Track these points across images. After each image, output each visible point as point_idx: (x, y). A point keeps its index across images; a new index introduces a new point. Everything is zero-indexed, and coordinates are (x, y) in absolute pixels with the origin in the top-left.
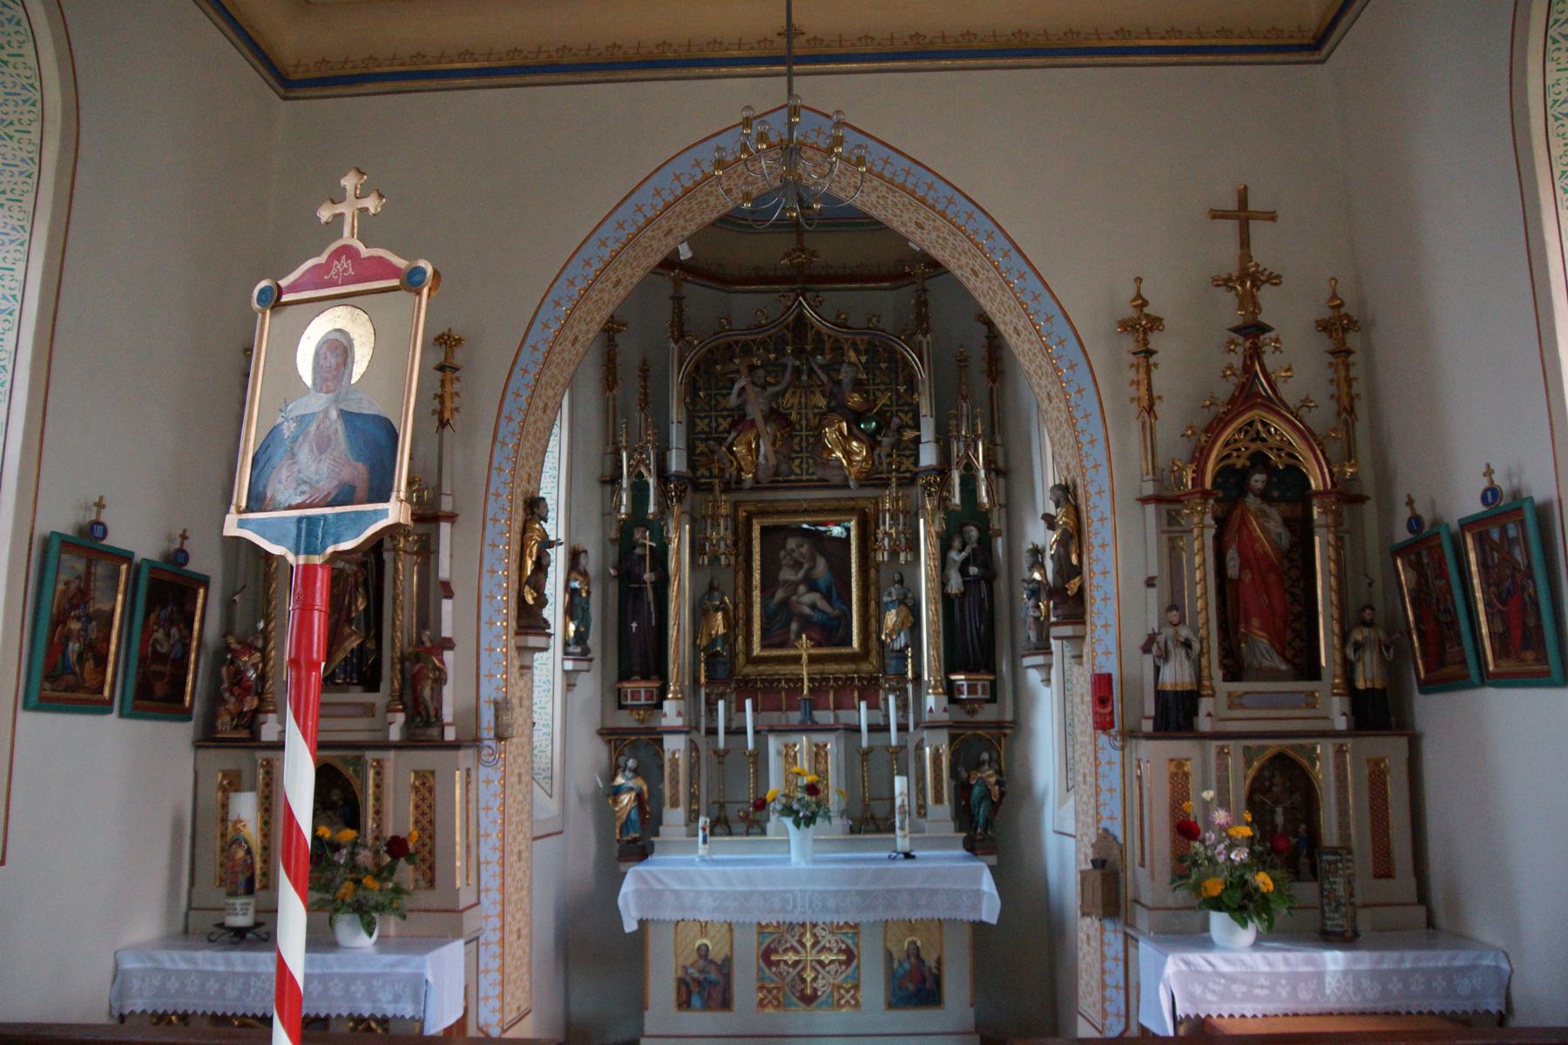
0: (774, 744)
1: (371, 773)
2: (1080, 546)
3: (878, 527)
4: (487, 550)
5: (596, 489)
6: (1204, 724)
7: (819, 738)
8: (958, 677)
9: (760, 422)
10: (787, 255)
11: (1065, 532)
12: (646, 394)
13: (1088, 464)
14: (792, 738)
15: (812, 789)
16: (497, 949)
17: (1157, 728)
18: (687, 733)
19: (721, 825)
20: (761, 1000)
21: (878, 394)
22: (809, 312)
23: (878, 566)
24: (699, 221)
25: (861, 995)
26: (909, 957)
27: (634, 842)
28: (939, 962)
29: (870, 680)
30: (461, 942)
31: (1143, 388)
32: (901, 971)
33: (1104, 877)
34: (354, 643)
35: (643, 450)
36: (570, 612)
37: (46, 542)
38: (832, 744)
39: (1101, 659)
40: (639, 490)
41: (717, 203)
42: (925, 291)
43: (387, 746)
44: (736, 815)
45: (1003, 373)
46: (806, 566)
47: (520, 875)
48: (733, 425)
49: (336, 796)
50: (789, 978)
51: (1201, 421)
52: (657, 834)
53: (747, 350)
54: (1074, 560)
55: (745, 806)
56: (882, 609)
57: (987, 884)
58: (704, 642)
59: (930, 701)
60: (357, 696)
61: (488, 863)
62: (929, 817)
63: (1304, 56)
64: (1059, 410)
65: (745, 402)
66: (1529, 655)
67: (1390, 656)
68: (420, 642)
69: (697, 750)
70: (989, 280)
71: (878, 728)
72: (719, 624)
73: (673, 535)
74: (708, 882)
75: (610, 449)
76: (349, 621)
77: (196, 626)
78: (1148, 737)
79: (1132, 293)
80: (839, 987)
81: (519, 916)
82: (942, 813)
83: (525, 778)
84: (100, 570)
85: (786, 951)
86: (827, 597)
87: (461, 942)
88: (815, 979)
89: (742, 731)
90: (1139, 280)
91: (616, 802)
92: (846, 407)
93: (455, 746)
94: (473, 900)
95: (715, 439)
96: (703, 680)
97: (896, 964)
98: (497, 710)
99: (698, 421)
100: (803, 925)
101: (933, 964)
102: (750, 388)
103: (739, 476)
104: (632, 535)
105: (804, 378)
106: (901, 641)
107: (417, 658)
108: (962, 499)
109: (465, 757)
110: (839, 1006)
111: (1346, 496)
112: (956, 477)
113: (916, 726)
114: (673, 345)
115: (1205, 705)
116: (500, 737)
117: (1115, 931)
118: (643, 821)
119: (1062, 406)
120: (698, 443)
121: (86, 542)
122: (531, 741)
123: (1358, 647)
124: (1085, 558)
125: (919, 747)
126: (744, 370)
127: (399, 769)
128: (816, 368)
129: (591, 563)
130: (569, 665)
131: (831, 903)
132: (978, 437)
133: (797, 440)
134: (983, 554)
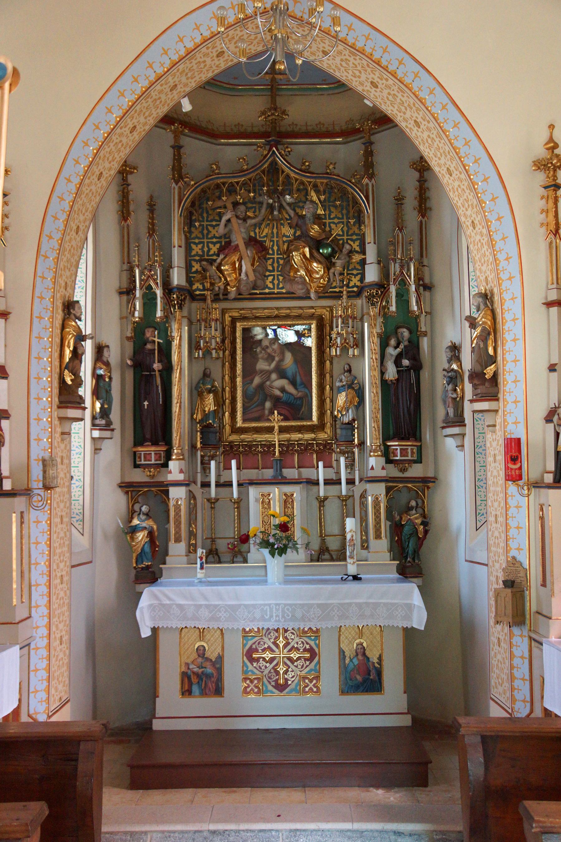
0: (253, 492)
2: (495, 341)
3: (331, 328)
4: (34, 341)
5: (116, 298)
7: (288, 489)
9: (242, 246)
10: (263, 113)
11: (484, 329)
12: (153, 224)
13: (503, 276)
14: (266, 489)
15: (284, 527)
16: (45, 653)
17: (556, 481)
18: (187, 485)
19: (213, 555)
20: (246, 688)
21: (333, 226)
22: (280, 161)
24: (197, 79)
26: (357, 655)
27: (146, 570)
28: (380, 658)
29: (325, 446)
30: (18, 647)
32: (351, 666)
33: (514, 594)
35: (151, 268)
36: (96, 393)
38: (296, 491)
39: (510, 427)
40: (149, 301)
41: (211, 67)
42: (371, 143)
44: (227, 550)
45: (430, 209)
46: (277, 359)
47: (62, 594)
48: (221, 250)
50: (266, 672)
52: (164, 563)
53: (232, 190)
54: (491, 351)
55: (232, 541)
57: (417, 599)
58: (199, 417)
59: (372, 461)
61: (37, 585)
62: (371, 549)
64: (481, 234)
65: (230, 231)
69: (194, 498)
70: (429, 129)
72: (210, 403)
73: (175, 334)
74: (206, 599)
75: (125, 267)
78: (549, 487)
79: (545, 137)
80: (304, 678)
81: (61, 626)
82: (381, 546)
83: (66, 520)
85: (264, 650)
86: (293, 383)
87: (18, 647)
88: (286, 672)
89: (229, 484)
91: (132, 539)
92: (309, 236)
93: (12, 494)
94: (26, 615)
95: (207, 260)
96: (199, 445)
97: (347, 661)
98: (44, 466)
99: (194, 246)
100: (277, 630)
101: (376, 660)
102: (234, 220)
103: (225, 289)
104: (144, 334)
105: (276, 213)
106: (350, 415)
108: (397, 307)
109: (19, 502)
110: (306, 693)
112: (393, 289)
113: (361, 480)
114: (174, 185)
116: (47, 488)
117: (521, 636)
118: (154, 552)
119: (485, 231)
120: (194, 263)
122: (69, 492)
124: (499, 350)
125: (363, 496)
126: (230, 206)
128: (285, 204)
129: (113, 355)
130: (96, 434)
131: (299, 614)
132: (411, 259)
133: (270, 262)
134: (412, 351)
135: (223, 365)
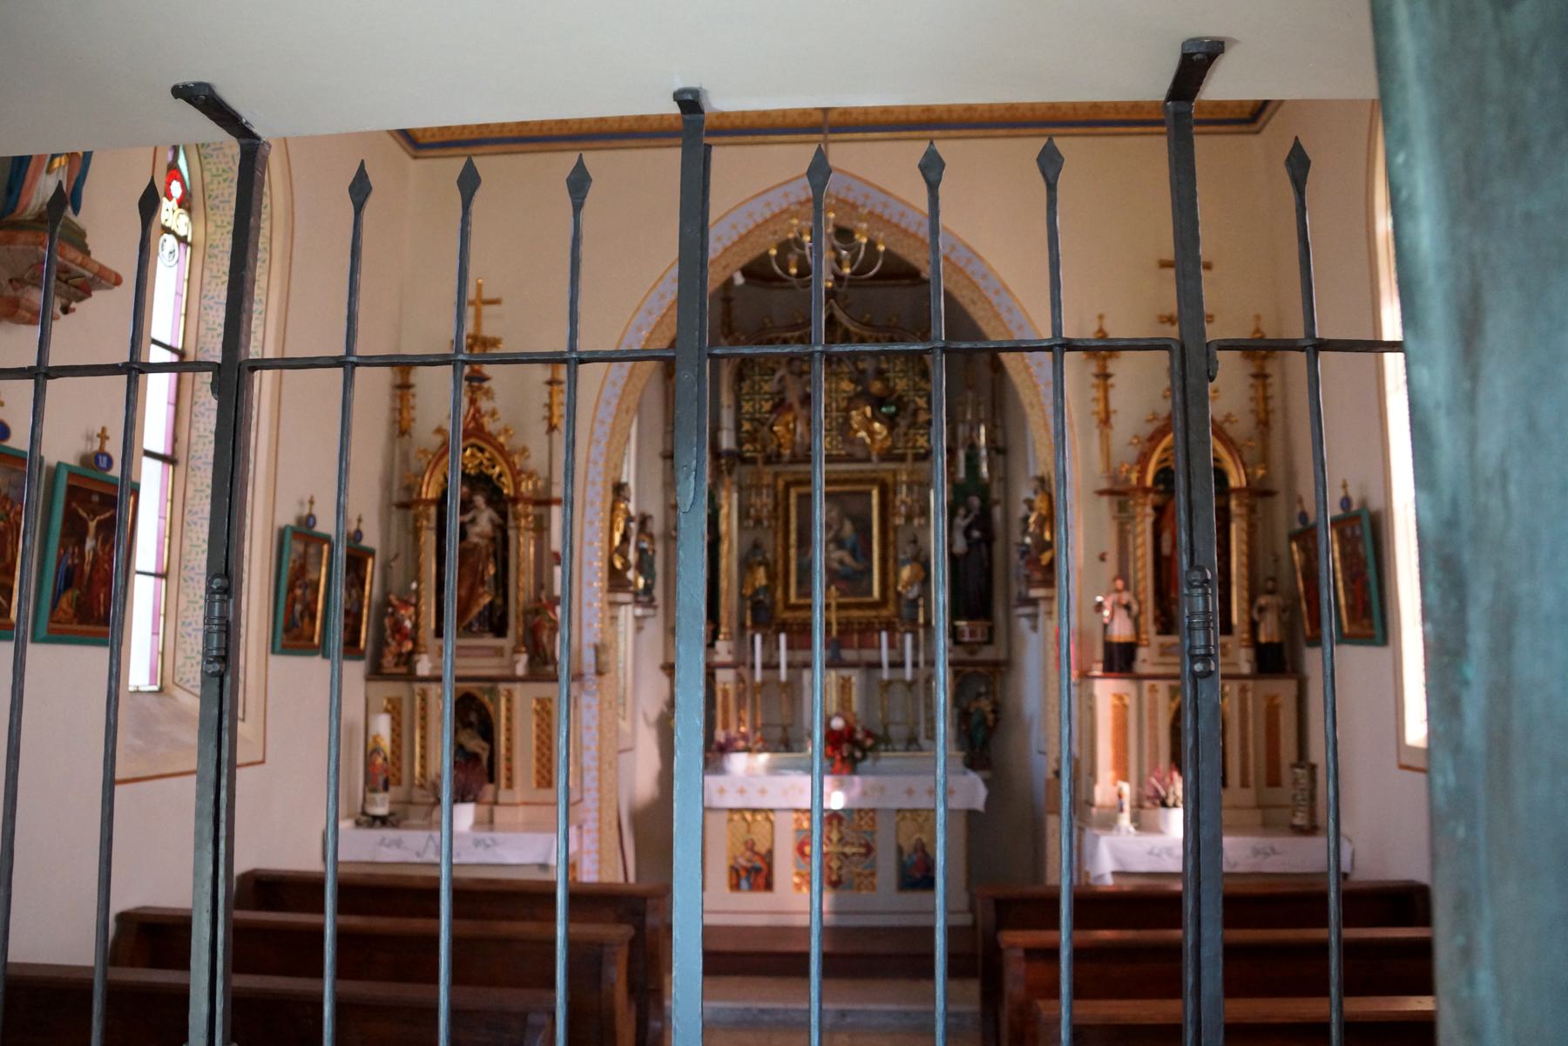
1: (503, 701)
6: (1141, 667)
7: (845, 672)
8: (962, 624)
9: (797, 405)
11: (1040, 515)
23: (896, 528)
25: (877, 880)
31: (1101, 405)
34: (486, 600)
37: (282, 533)
38: (855, 676)
43: (513, 679)
49: (473, 717)
51: (1150, 429)
56: (899, 564)
60: (489, 641)
63: (1244, 128)
66: (1366, 622)
67: (1286, 616)
68: (540, 600)
71: (897, 664)
72: (761, 577)
76: (483, 583)
77: (367, 587)
80: (859, 875)
84: (312, 550)
86: (853, 553)
88: (840, 868)
90: (1101, 317)
96: (749, 623)
102: (789, 378)
107: (537, 612)
111: (1259, 492)
115: (1142, 653)
121: (304, 530)
123: (1262, 610)
127: (524, 697)
134: (983, 520)
135: (776, 534)
